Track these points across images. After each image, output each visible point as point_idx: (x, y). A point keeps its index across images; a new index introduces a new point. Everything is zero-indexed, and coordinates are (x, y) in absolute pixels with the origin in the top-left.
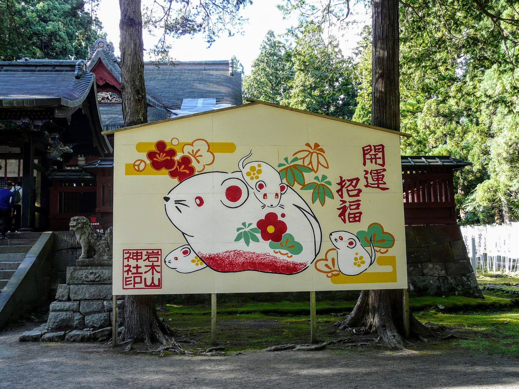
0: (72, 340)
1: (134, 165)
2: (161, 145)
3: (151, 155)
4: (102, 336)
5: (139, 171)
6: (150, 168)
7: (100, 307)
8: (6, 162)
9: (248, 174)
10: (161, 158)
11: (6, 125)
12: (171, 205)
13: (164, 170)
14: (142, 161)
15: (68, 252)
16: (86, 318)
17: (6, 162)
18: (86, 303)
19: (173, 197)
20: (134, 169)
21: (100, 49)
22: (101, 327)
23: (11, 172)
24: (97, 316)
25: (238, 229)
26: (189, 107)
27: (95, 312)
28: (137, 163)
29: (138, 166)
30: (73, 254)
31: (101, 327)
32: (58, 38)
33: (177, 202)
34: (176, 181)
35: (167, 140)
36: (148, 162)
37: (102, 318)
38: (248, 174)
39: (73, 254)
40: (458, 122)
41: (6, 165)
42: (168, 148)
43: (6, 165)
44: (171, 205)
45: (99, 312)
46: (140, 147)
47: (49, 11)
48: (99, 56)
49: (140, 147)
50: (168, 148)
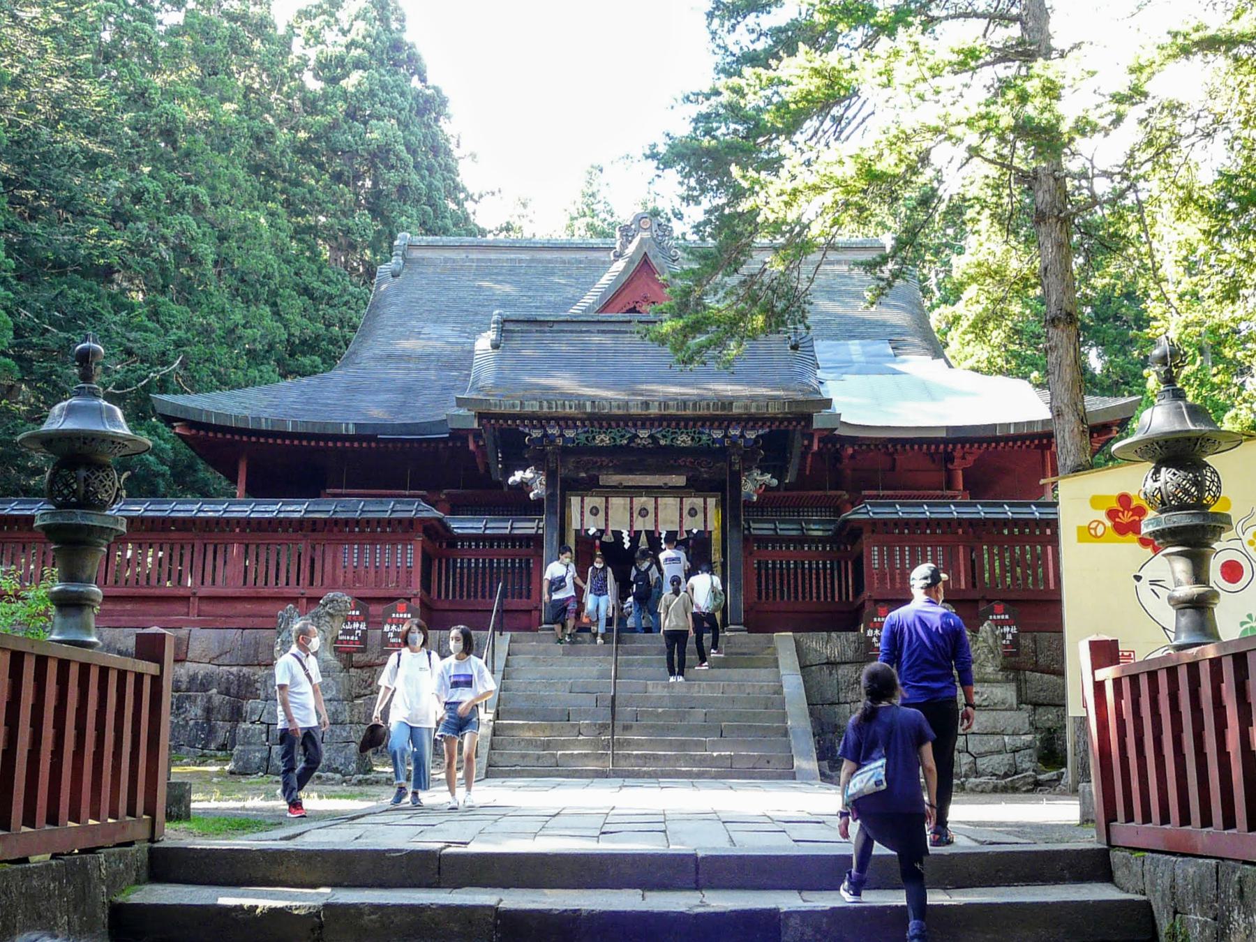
0: (980, 789)
1: (1089, 528)
2: (1124, 499)
3: (1112, 514)
4: (1024, 785)
5: (1096, 536)
6: (1112, 533)
7: (1001, 745)
8: (656, 502)
9: (1251, 543)
10: (1126, 518)
11: (693, 439)
12: (1144, 586)
13: (1130, 536)
14: (1100, 522)
15: (821, 669)
16: (978, 761)
17: (656, 502)
18: (978, 737)
19: (1147, 574)
20: (1088, 534)
21: (646, 235)
22: (1006, 775)
23: (665, 522)
24: (996, 758)
25: (1242, 624)
26: (834, 361)
27: (992, 753)
28: (1093, 526)
29: (1095, 529)
30: (831, 674)
31: (1006, 775)
32: (393, 160)
33: (1153, 582)
34: (1149, 551)
35: (1133, 493)
36: (1109, 524)
37: (1006, 761)
38: (1251, 543)
39: (831, 674)
40: (974, 152)
41: (656, 508)
42: (1134, 503)
43: (656, 508)
44: (1144, 586)
45: (999, 752)
46: (1095, 502)
47: (372, 94)
48: (645, 250)
49: (1095, 502)
50: (1134, 503)
